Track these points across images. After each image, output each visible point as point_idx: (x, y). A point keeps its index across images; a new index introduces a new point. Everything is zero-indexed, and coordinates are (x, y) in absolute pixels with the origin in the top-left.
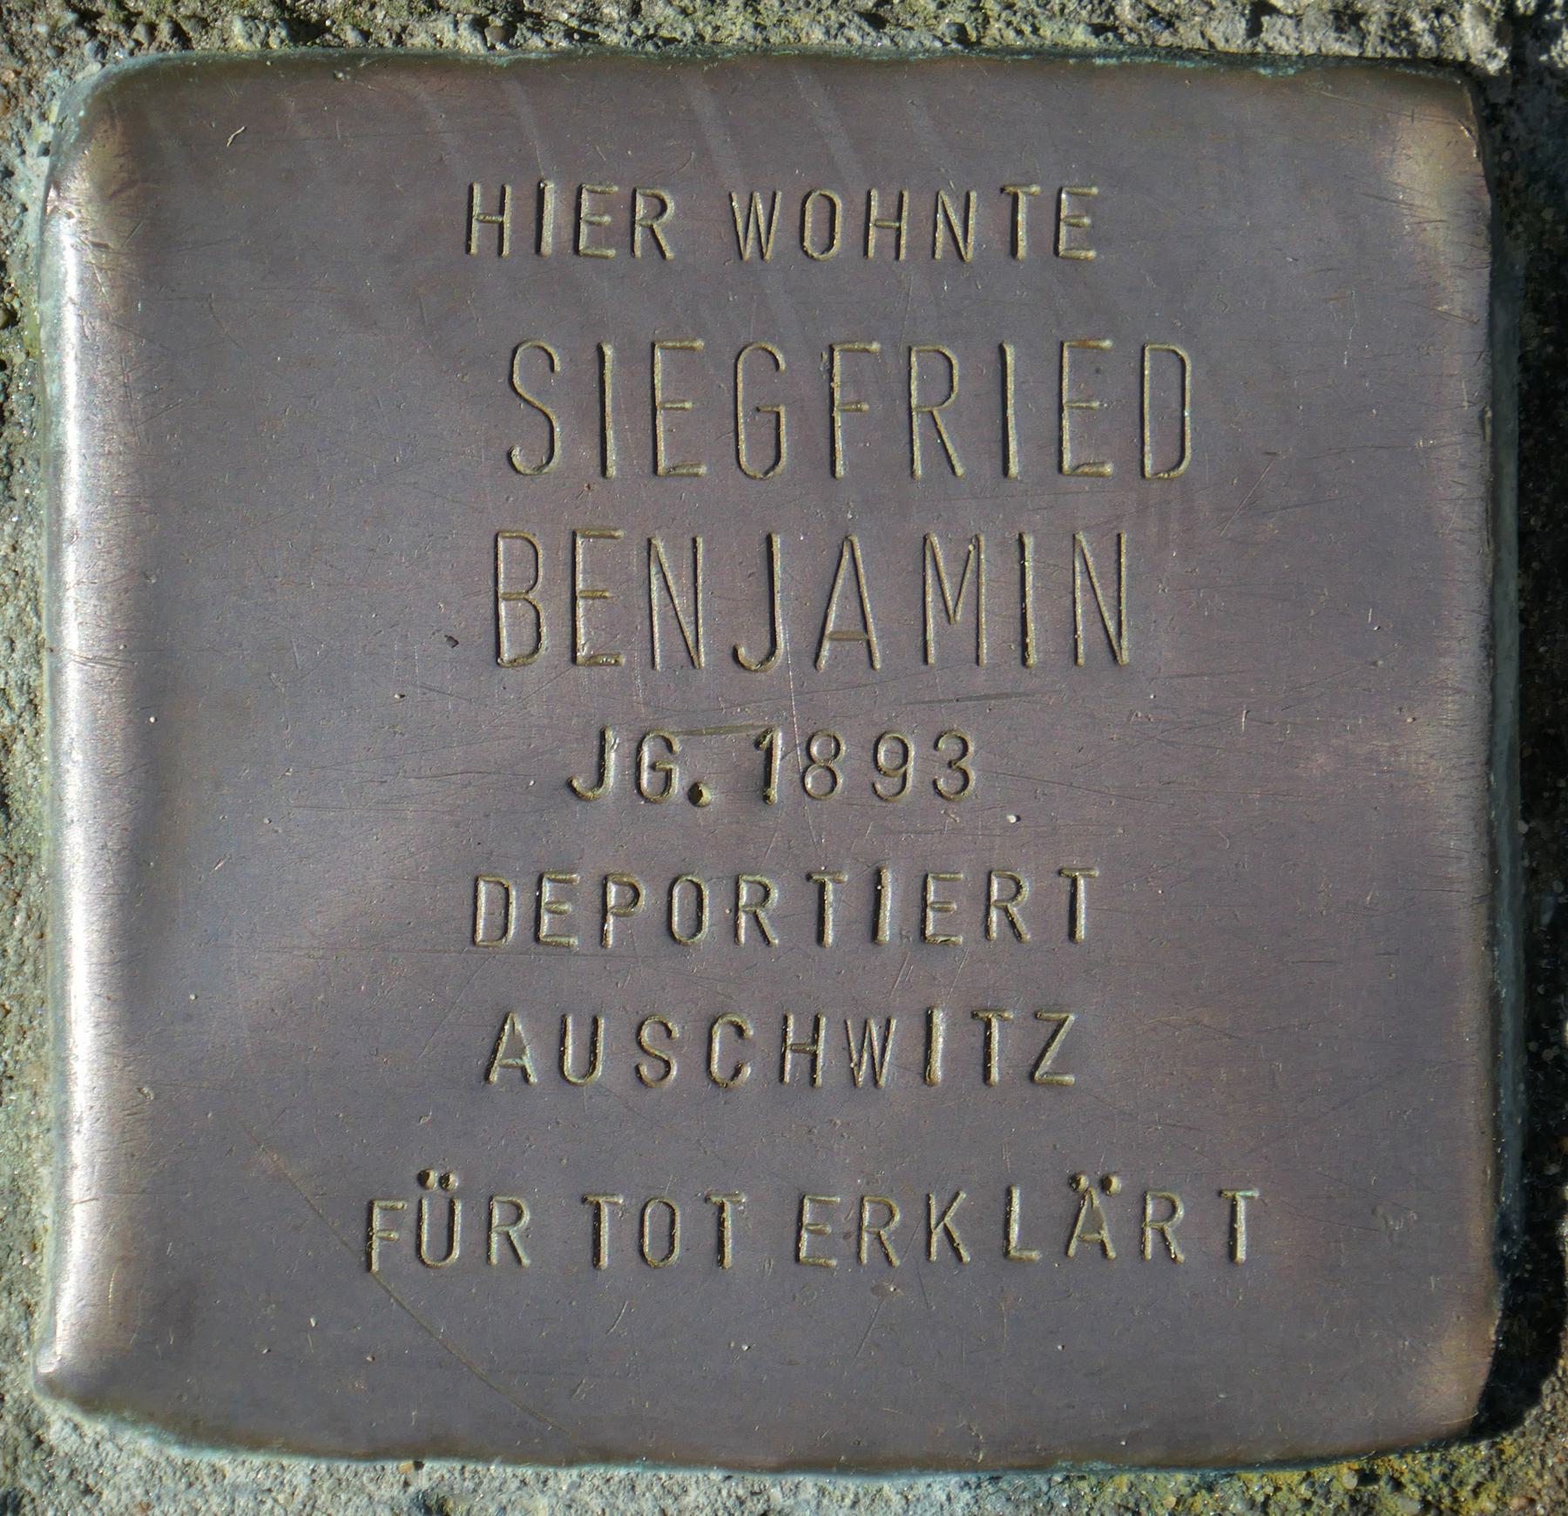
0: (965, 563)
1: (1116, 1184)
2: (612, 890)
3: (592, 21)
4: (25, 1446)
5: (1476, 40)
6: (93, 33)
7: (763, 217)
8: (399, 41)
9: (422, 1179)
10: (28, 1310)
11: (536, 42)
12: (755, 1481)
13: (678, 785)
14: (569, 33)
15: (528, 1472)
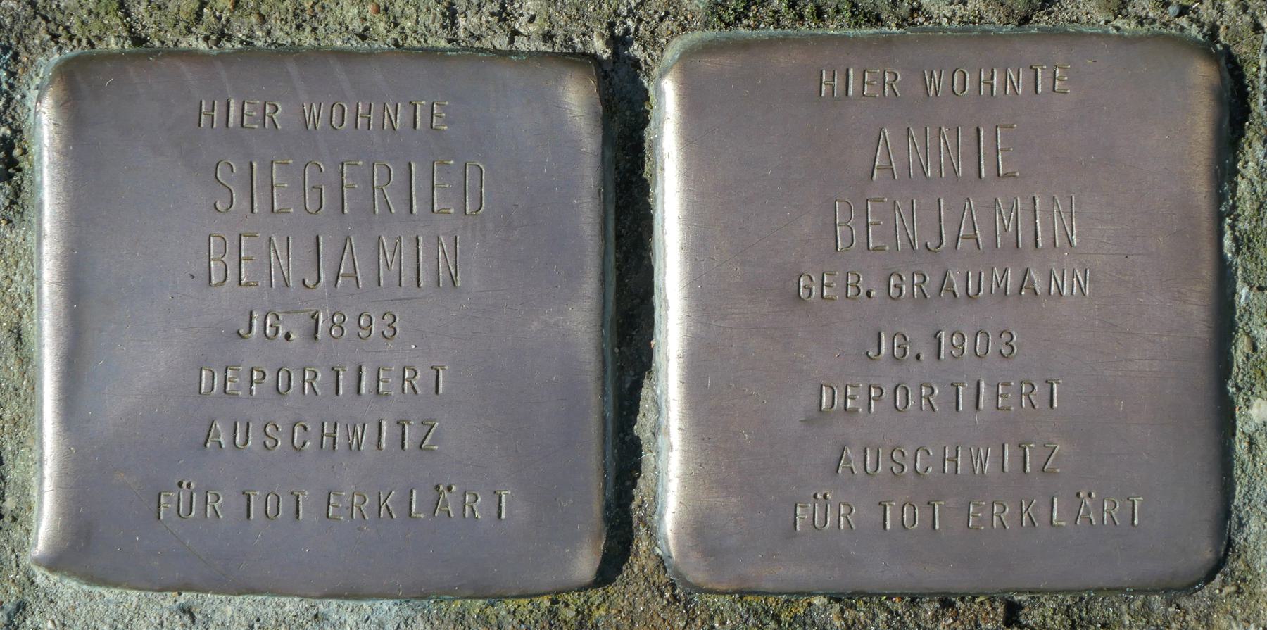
0: (396, 247)
1: (454, 488)
2: (255, 373)
3: (251, 37)
4: (28, 584)
5: (598, 46)
6: (57, 43)
7: (318, 113)
8: (176, 45)
9: (180, 484)
10: (28, 532)
11: (229, 45)
12: (313, 601)
13: (281, 332)
14: (241, 42)
15: (223, 597)
